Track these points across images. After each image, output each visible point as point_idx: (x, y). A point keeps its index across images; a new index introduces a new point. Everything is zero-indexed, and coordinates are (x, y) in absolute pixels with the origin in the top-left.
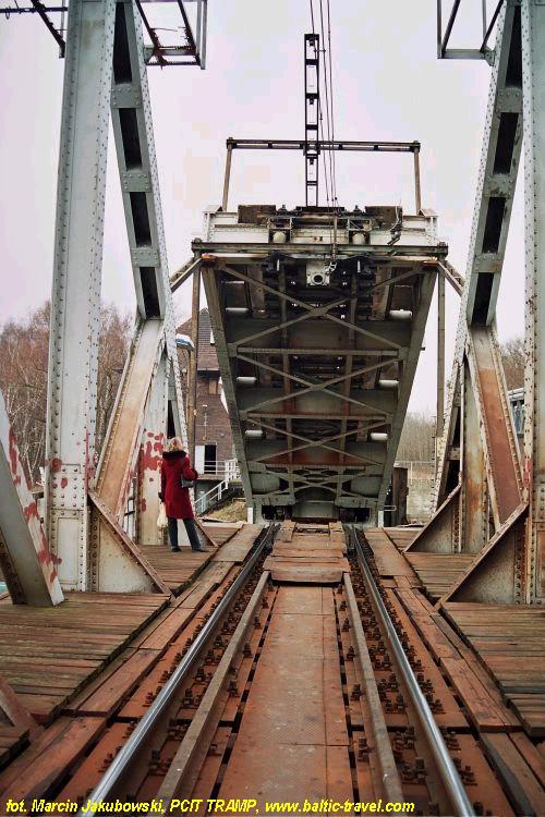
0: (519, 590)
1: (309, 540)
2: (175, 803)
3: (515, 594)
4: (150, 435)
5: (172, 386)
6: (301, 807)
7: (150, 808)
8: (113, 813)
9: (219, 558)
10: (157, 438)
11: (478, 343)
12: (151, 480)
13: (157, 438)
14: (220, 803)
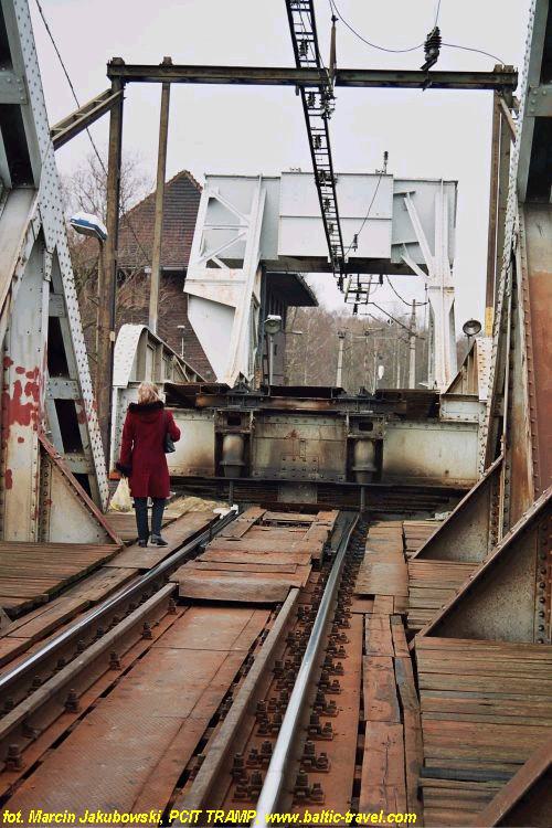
0: (543, 622)
1: (270, 538)
2: (175, 814)
3: (537, 628)
4: (20, 370)
5: (55, 289)
6: (302, 817)
7: (148, 818)
8: (112, 824)
9: (117, 563)
10: (30, 375)
11: (534, 232)
12: (21, 440)
13: (30, 375)
14: (220, 814)
